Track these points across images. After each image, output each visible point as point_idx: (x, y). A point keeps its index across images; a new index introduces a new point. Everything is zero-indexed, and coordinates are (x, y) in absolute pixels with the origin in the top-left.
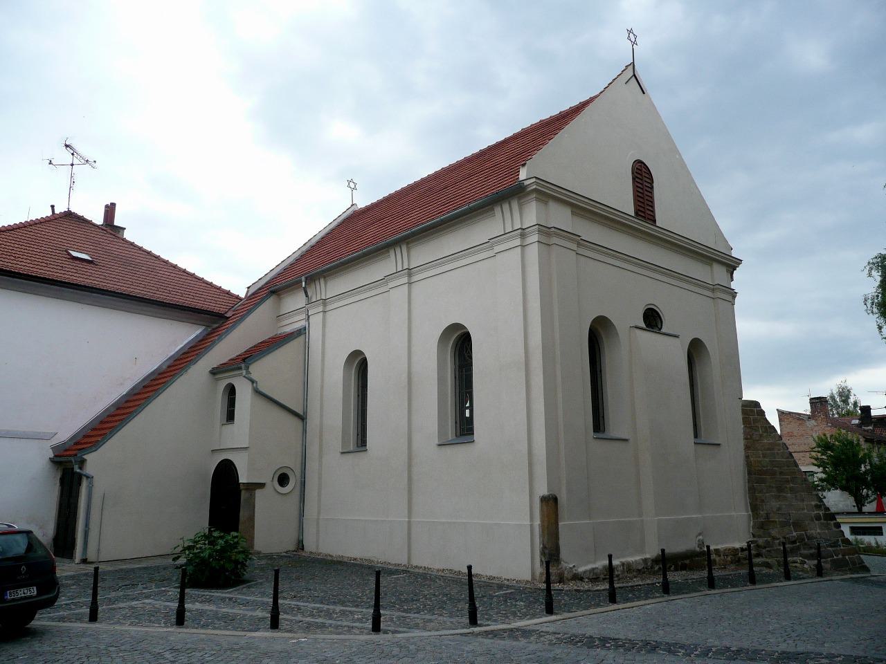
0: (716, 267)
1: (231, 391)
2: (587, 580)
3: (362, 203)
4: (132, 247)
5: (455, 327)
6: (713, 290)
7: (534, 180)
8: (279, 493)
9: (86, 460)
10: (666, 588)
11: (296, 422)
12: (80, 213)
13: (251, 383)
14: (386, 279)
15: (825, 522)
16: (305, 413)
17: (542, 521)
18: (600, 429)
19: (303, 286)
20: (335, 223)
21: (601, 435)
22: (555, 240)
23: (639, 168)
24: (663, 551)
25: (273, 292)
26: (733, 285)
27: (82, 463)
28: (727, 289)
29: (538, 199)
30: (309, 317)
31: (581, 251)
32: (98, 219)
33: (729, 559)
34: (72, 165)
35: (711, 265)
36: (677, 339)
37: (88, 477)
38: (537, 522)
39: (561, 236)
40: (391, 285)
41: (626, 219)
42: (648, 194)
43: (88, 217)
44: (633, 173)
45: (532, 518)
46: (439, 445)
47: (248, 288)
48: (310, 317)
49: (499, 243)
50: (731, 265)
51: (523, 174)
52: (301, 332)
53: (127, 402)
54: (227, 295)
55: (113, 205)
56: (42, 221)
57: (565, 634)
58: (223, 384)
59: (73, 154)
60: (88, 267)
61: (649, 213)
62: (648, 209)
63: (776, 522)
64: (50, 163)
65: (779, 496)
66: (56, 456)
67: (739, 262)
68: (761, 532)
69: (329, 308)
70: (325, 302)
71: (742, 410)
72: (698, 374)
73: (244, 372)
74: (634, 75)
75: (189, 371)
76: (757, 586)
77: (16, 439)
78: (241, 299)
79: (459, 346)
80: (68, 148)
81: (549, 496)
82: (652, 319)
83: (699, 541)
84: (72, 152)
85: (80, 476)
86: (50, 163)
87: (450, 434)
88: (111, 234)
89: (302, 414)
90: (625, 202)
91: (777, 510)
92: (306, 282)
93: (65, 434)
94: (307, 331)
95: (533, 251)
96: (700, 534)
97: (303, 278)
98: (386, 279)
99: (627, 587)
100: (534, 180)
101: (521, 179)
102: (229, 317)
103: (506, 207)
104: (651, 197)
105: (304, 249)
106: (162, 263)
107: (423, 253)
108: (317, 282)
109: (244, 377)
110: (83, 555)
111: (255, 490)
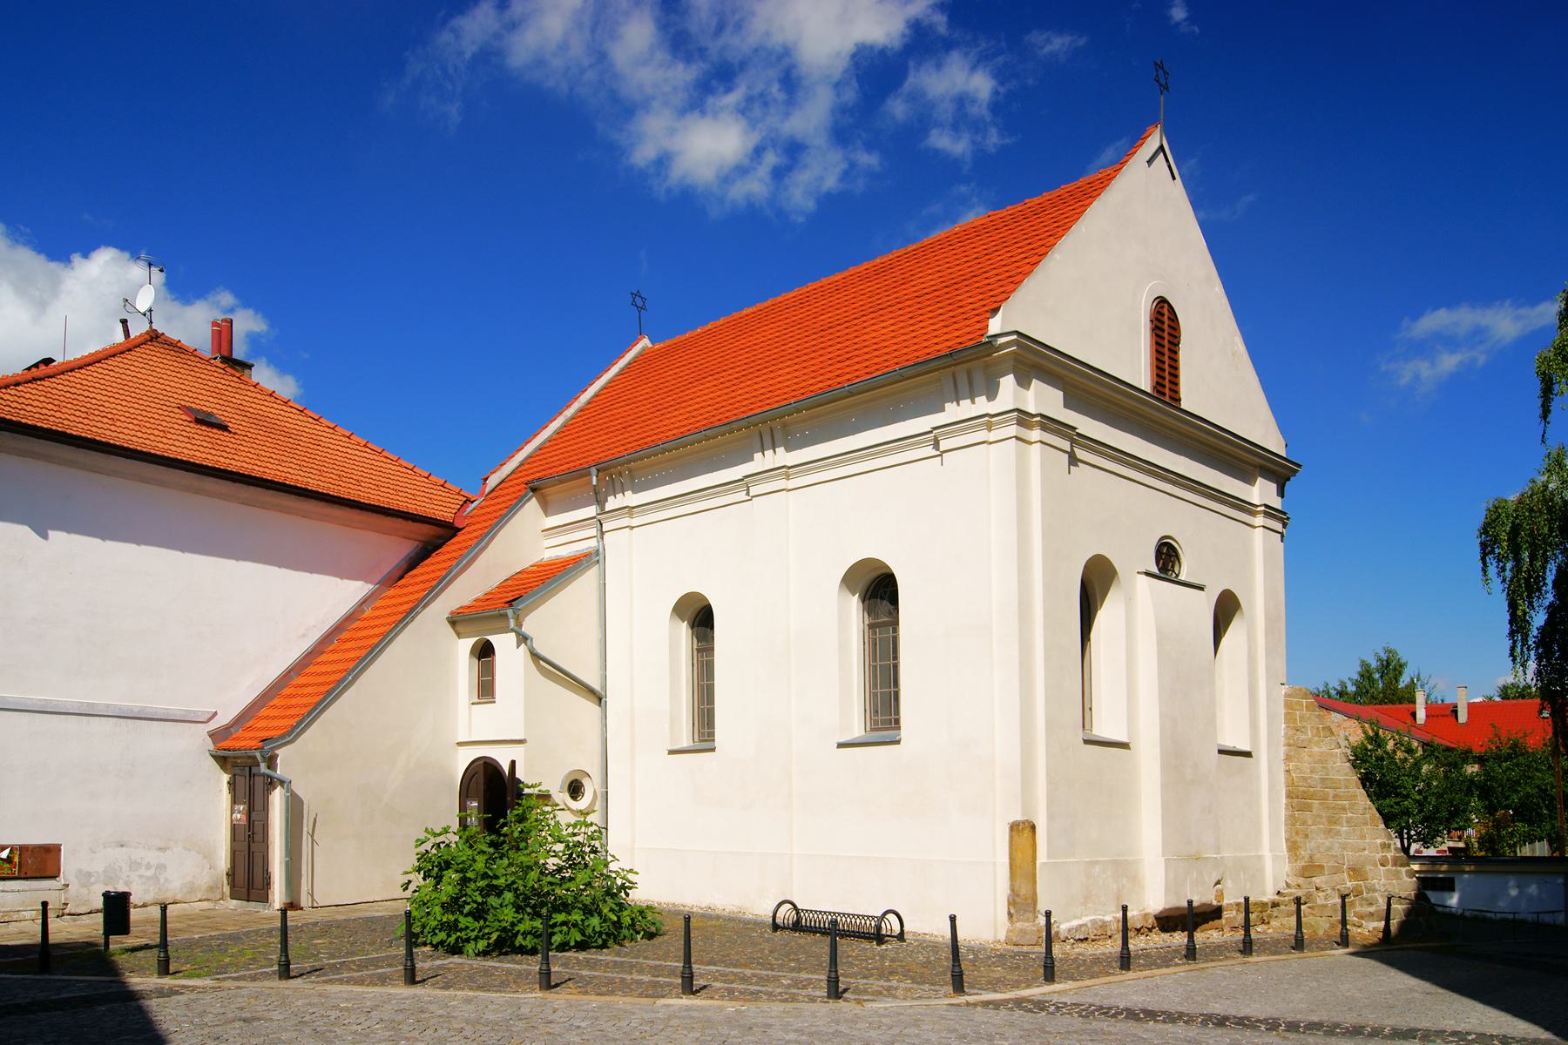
1: (485, 652)
4: (273, 399)
10: (1191, 953)
11: (591, 707)
15: (1394, 868)
16: (604, 686)
27: (271, 762)
30: (603, 533)
37: (282, 783)
52: (591, 559)
58: (467, 644)
65: (1330, 830)
68: (1301, 881)
71: (1286, 702)
81: (1024, 822)
82: (1167, 557)
90: (1139, 373)
91: (1326, 851)
93: (224, 719)
94: (601, 556)
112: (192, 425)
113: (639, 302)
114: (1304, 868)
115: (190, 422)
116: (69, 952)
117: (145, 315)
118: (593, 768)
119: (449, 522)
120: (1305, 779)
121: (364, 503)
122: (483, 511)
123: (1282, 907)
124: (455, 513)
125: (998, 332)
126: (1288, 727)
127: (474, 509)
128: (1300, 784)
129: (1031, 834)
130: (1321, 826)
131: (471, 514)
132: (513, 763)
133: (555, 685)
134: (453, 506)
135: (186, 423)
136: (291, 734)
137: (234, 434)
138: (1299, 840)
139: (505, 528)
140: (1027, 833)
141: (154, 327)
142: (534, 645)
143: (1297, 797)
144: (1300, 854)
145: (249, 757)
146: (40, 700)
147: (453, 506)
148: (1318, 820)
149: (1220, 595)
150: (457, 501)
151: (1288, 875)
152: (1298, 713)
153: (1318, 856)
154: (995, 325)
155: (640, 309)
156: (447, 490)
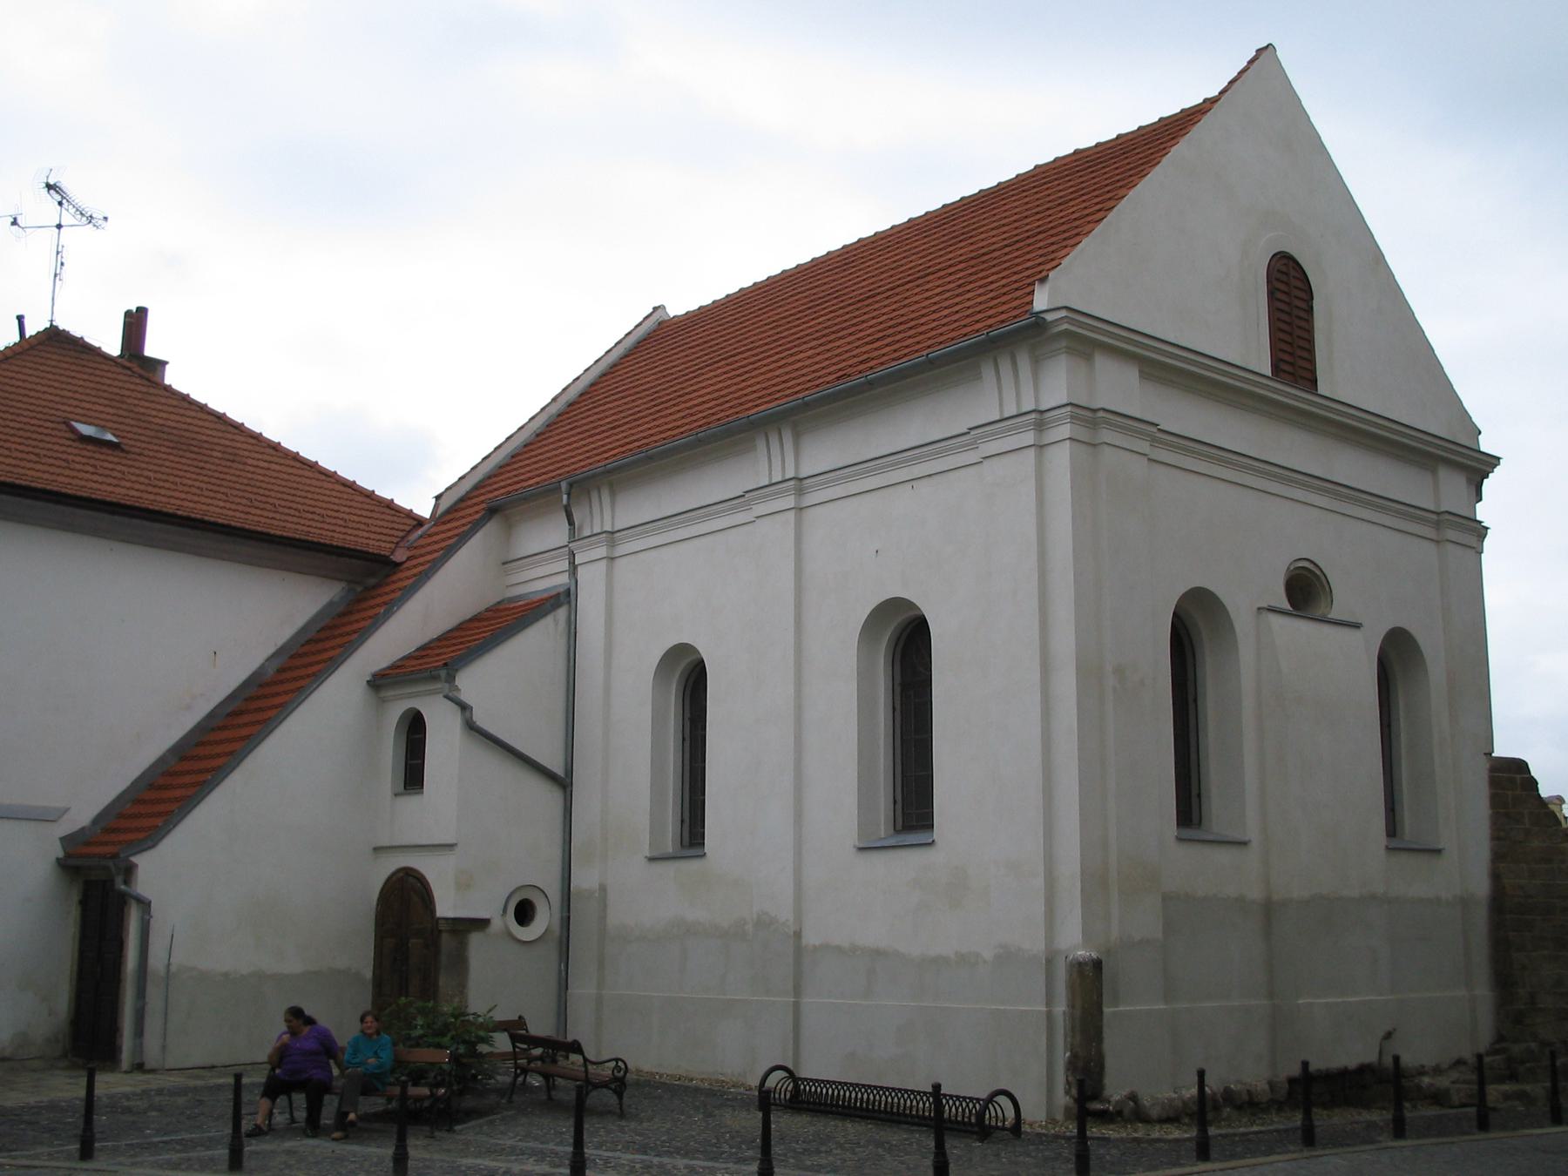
0: (1443, 473)
1: (414, 727)
7: (1063, 313)
10: (1309, 1138)
11: (549, 796)
12: (76, 331)
17: (1072, 1006)
18: (1191, 821)
20: (620, 351)
21: (1189, 833)
22: (1107, 435)
24: (1305, 1064)
25: (493, 512)
26: (1483, 512)
27: (129, 871)
28: (1464, 522)
29: (1070, 351)
32: (112, 344)
34: (59, 226)
35: (1434, 472)
38: (1061, 1008)
42: (1303, 324)
45: (1050, 1000)
46: (861, 849)
47: (438, 498)
48: (579, 568)
50: (1478, 467)
51: (1041, 301)
54: (388, 511)
56: (9, 353)
59: (60, 204)
61: (1301, 343)
62: (1300, 327)
64: (15, 223)
66: (68, 855)
67: (1492, 462)
70: (612, 536)
76: (1491, 1135)
78: (419, 522)
80: (52, 192)
84: (59, 198)
86: (15, 223)
88: (141, 376)
92: (569, 494)
93: (82, 815)
94: (573, 597)
95: (1061, 459)
97: (564, 485)
98: (741, 500)
99: (1235, 1135)
100: (1063, 313)
102: (401, 564)
103: (1005, 366)
104: (1308, 331)
105: (554, 410)
108: (594, 496)
115: (74, 441)
118: (550, 883)
119: (384, 556)
122: (429, 540)
124: (397, 543)
125: (1045, 308)
127: (421, 536)
131: (415, 545)
134: (396, 533)
136: (151, 836)
137: (127, 452)
139: (1394, 419)
141: (54, 323)
142: (474, 719)
147: (396, 533)
152: (1510, 793)
154: (1041, 300)
156: (393, 512)
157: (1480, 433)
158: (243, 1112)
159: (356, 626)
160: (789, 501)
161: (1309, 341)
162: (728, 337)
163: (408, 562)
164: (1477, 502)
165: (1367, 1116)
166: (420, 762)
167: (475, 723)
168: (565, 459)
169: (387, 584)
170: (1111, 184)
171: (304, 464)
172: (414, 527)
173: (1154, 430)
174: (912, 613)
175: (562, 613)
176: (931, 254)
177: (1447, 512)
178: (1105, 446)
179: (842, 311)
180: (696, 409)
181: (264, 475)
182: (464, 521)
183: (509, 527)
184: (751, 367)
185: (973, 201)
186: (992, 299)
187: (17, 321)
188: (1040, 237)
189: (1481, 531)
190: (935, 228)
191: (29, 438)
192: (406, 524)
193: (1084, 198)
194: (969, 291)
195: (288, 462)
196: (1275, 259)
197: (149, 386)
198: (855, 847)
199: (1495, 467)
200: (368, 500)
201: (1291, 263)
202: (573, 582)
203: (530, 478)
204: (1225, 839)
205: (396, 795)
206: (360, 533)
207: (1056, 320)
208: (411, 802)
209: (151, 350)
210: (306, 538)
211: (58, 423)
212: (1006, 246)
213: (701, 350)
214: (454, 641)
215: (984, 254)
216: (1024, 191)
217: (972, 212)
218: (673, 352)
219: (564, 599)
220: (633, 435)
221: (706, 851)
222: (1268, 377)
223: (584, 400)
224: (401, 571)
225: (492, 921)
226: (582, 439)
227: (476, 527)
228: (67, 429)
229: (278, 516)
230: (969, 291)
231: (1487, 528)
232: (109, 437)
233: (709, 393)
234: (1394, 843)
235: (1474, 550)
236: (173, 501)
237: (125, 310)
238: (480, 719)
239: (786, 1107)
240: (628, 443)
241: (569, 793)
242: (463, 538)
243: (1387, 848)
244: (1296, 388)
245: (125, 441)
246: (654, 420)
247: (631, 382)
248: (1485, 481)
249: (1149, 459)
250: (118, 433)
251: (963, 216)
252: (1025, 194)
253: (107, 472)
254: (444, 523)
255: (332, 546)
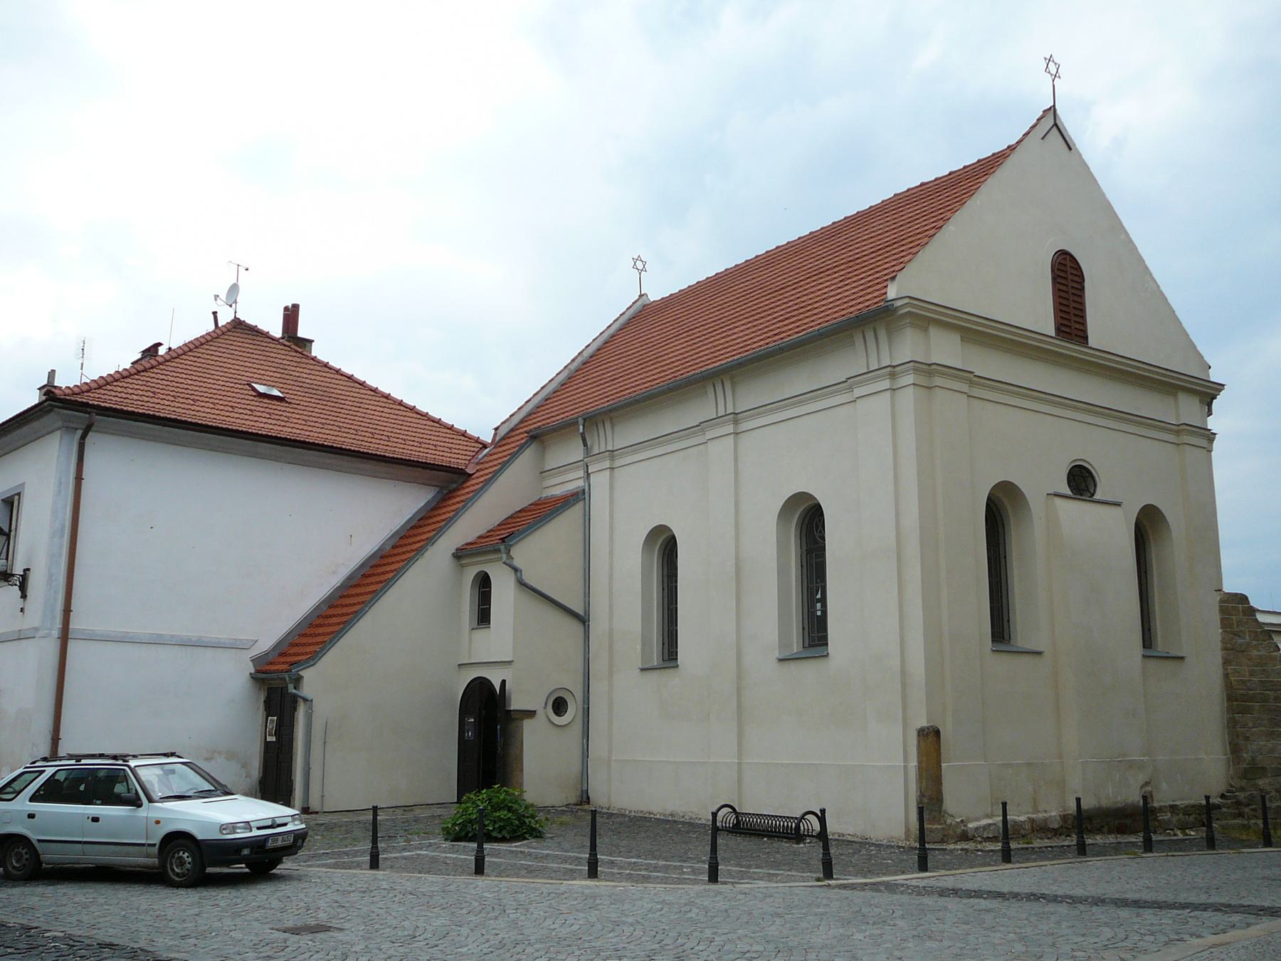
0: (1182, 397)
1: (484, 583)
2: (979, 839)
3: (656, 294)
4: (327, 370)
5: (799, 499)
6: (1178, 433)
7: (907, 300)
8: (553, 723)
9: (302, 677)
10: (1082, 850)
11: (577, 627)
13: (513, 571)
14: (702, 426)
16: (587, 612)
17: (920, 762)
19: (581, 431)
22: (938, 381)
23: (1063, 262)
26: (1212, 423)
27: (298, 681)
30: (588, 475)
31: (976, 392)
32: (276, 330)
33: (1192, 818)
35: (1175, 396)
36: (1118, 508)
37: (305, 700)
38: (913, 763)
39: (944, 374)
40: (709, 435)
41: (1044, 342)
43: (263, 327)
44: (1052, 271)
45: (906, 759)
47: (496, 429)
49: (861, 384)
50: (1207, 393)
51: (892, 292)
52: (579, 496)
53: (342, 597)
54: (462, 438)
55: (296, 307)
57: (957, 927)
58: (471, 573)
60: (279, 408)
63: (1267, 768)
66: (257, 671)
68: (1244, 783)
69: (618, 463)
70: (612, 454)
72: (1153, 556)
73: (504, 556)
74: (1056, 124)
75: (426, 555)
77: (209, 648)
79: (806, 522)
81: (928, 728)
83: (1145, 792)
85: (295, 700)
87: (796, 647)
88: (296, 351)
89: (582, 613)
92: (584, 426)
93: (266, 643)
95: (908, 398)
96: (1147, 784)
98: (702, 426)
100: (907, 300)
101: (889, 298)
106: (369, 392)
107: (753, 394)
109: (504, 563)
110: (303, 803)
111: (523, 720)
112: (255, 399)
113: (640, 265)
114: (1246, 771)
115: (255, 396)
116: (156, 871)
117: (231, 306)
119: (462, 469)
120: (1244, 682)
121: (389, 457)
123: (1224, 810)
124: (470, 460)
126: (1224, 631)
127: (486, 455)
128: (1239, 687)
129: (934, 738)
130: (1263, 729)
131: (481, 461)
132: (504, 682)
133: (571, 608)
135: (252, 398)
136: (313, 658)
137: (290, 403)
138: (1240, 742)
140: (931, 738)
141: (237, 316)
143: (1236, 700)
144: (1242, 756)
145: (281, 679)
146: (120, 632)
148: (1259, 722)
149: (1158, 508)
150: (473, 449)
151: (1232, 778)
153: (1260, 757)
155: (640, 271)
156: (467, 439)
157: (1210, 368)
158: (379, 835)
159: (443, 517)
160: (730, 429)
161: (1082, 310)
162: (668, 333)
163: (477, 473)
164: (1208, 416)
165: (1132, 839)
166: (488, 606)
167: (523, 580)
168: (580, 402)
169: (464, 488)
170: (943, 208)
171: (407, 408)
172: (481, 448)
173: (971, 376)
174: (815, 502)
175: (579, 506)
176: (824, 258)
177: (1185, 424)
178: (937, 388)
179: (727, 314)
180: (667, 367)
181: (381, 416)
182: (513, 445)
183: (544, 448)
184: (721, 330)
185: (853, 220)
186: (862, 290)
187: (212, 316)
188: (895, 246)
189: (1210, 437)
190: (826, 239)
191: (218, 390)
192: (474, 447)
193: (924, 218)
194: (847, 285)
195: (394, 407)
196: (1056, 255)
197: (302, 358)
198: (777, 659)
199: (1220, 391)
200: (449, 431)
201: (1068, 257)
202: (587, 484)
203: (558, 415)
204: (1023, 650)
205: (473, 629)
206: (445, 454)
207: (902, 305)
208: (481, 634)
209: (301, 333)
210: (368, 451)
211: (244, 384)
212: (872, 252)
213: (671, 326)
214: (509, 526)
215: (858, 258)
216: (886, 213)
217: (852, 228)
218: (652, 326)
219: (579, 496)
220: (626, 385)
221: (679, 663)
222: (1051, 337)
223: (593, 361)
224: (473, 479)
225: (537, 712)
226: (628, 365)
227: (522, 448)
228: (250, 388)
229: (390, 444)
230: (847, 285)
231: (1215, 434)
232: (276, 392)
233: (664, 360)
234: (1149, 653)
235: (1205, 450)
236: (321, 436)
237: (284, 306)
238: (528, 578)
239: (730, 832)
240: (622, 391)
241: (587, 626)
242: (514, 456)
243: (1144, 656)
244: (1071, 343)
245: (288, 396)
246: (640, 374)
247: (624, 348)
248: (1214, 401)
249: (968, 396)
250: (282, 390)
251: (845, 231)
252: (887, 215)
253: (278, 417)
254: (500, 446)
255: (426, 463)
